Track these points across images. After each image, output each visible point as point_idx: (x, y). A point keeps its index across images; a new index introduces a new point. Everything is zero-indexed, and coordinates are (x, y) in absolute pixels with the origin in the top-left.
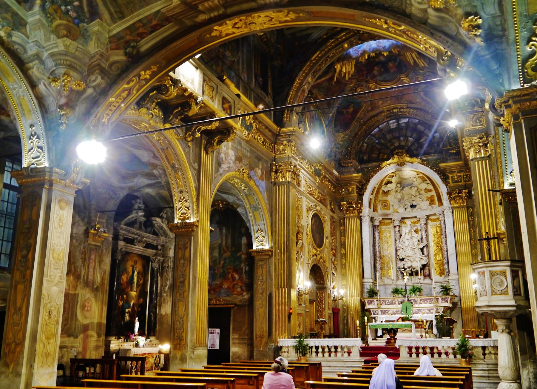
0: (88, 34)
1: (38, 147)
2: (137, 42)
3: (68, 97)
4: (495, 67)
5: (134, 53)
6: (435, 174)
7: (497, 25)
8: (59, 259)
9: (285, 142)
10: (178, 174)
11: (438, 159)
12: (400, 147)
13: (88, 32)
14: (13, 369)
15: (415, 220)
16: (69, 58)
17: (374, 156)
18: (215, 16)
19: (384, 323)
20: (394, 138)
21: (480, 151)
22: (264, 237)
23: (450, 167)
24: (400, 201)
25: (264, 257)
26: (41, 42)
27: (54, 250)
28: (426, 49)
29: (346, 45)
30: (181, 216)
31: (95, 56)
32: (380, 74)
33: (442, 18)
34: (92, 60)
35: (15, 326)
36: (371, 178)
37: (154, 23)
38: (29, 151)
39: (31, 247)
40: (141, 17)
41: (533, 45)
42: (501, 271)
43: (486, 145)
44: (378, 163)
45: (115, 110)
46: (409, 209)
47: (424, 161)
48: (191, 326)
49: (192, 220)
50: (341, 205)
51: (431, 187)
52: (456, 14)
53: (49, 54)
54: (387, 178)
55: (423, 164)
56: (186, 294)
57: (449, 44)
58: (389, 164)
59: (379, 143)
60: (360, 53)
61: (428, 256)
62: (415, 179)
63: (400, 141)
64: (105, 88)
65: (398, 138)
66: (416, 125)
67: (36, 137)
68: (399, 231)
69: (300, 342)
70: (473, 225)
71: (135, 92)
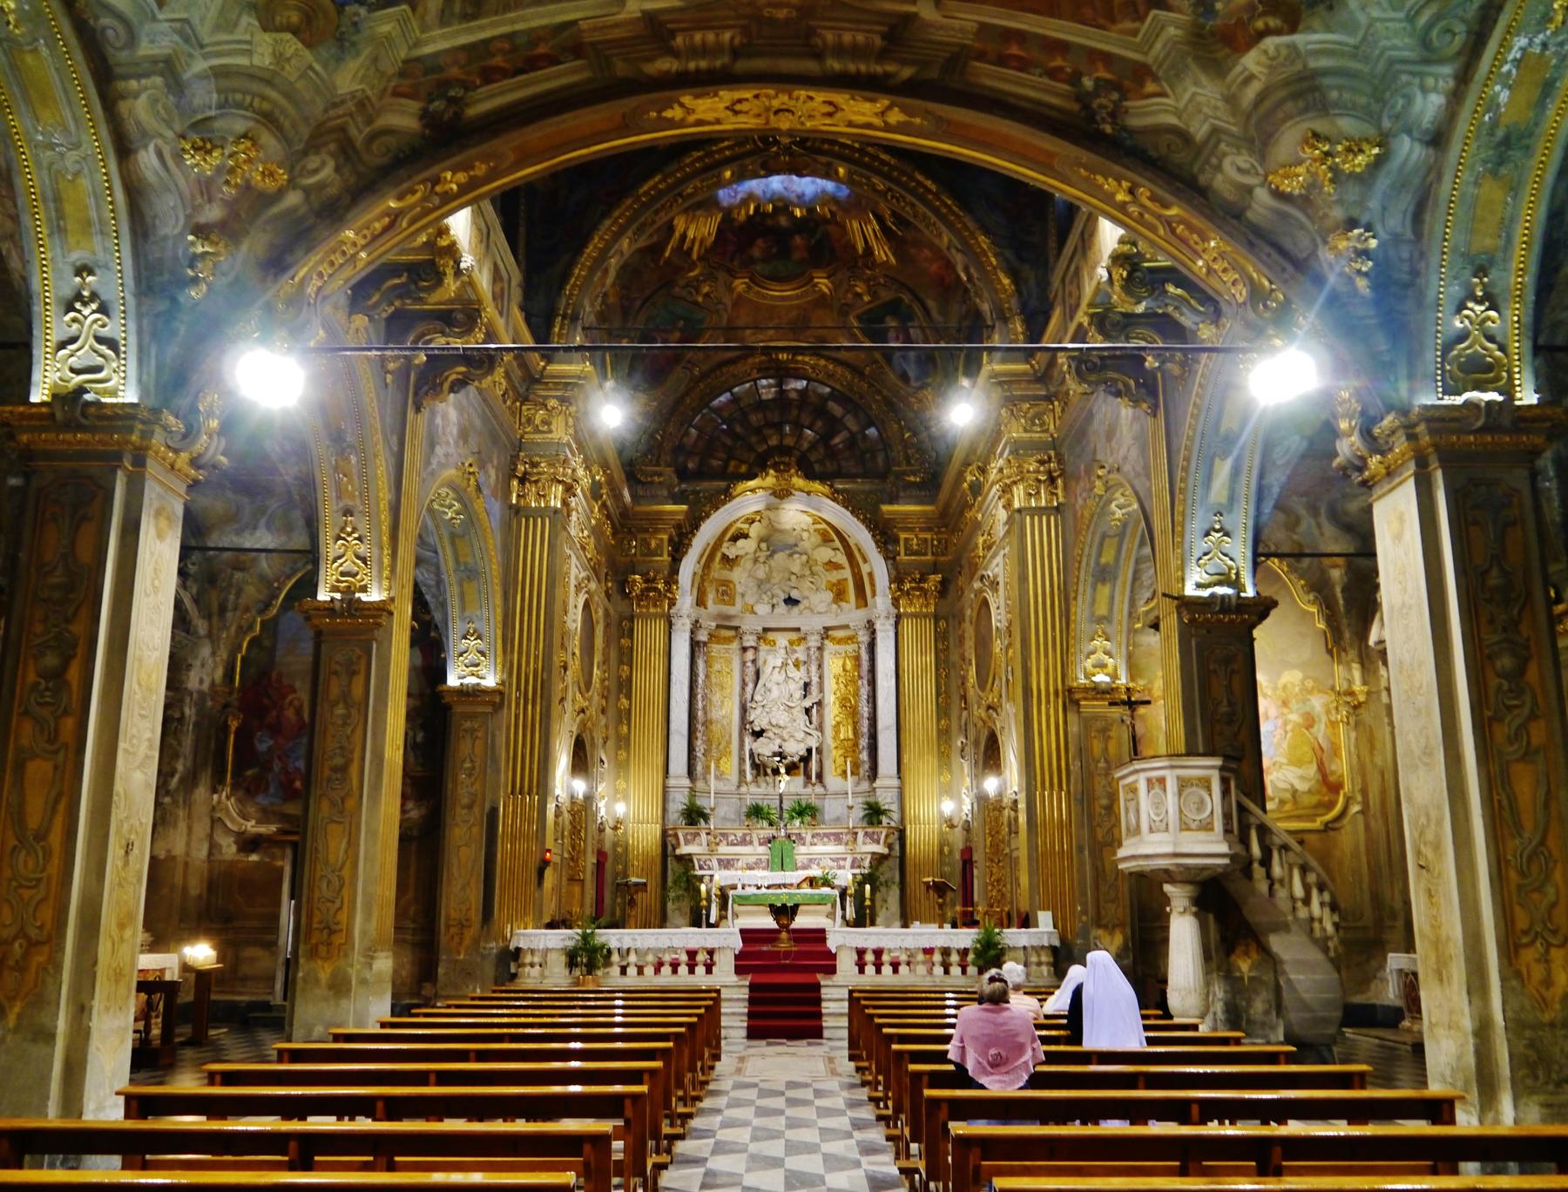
0: (354, 38)
1: (100, 340)
2: (467, 89)
3: (231, 205)
4: (1384, 347)
5: (446, 117)
6: (863, 527)
7: (1401, 260)
8: (149, 689)
9: (552, 403)
10: (347, 459)
11: (870, 492)
12: (783, 450)
13: (358, 31)
14: (20, 1017)
15: (794, 636)
16: (274, 94)
17: (715, 463)
18: (698, 71)
19: (764, 890)
20: (770, 425)
21: (1038, 493)
22: (482, 653)
23: (907, 514)
24: (760, 584)
25: (480, 709)
26: (199, 28)
27: (140, 660)
28: (1210, 271)
29: (728, 174)
30: (338, 581)
31: (343, 102)
32: (766, 260)
33: (1284, 216)
34: (332, 113)
35: (21, 886)
36: (703, 519)
37: (542, 49)
38: (62, 345)
39: (75, 646)
40: (519, 27)
41: (1467, 317)
42: (1200, 779)
43: (1052, 480)
44: (723, 484)
45: (341, 265)
46: (782, 608)
47: (837, 491)
48: (364, 890)
49: (374, 595)
50: (626, 581)
51: (841, 558)
52: (1326, 216)
53: (211, 68)
54: (739, 525)
55: (834, 500)
56: (350, 803)
57: (1286, 276)
58: (753, 491)
59: (730, 433)
60: (739, 197)
61: (820, 728)
62: (805, 535)
63: (782, 436)
64: (338, 198)
65: (778, 427)
66: (824, 399)
67: (94, 306)
68: (754, 661)
69: (585, 937)
70: (946, 661)
71: (404, 224)
